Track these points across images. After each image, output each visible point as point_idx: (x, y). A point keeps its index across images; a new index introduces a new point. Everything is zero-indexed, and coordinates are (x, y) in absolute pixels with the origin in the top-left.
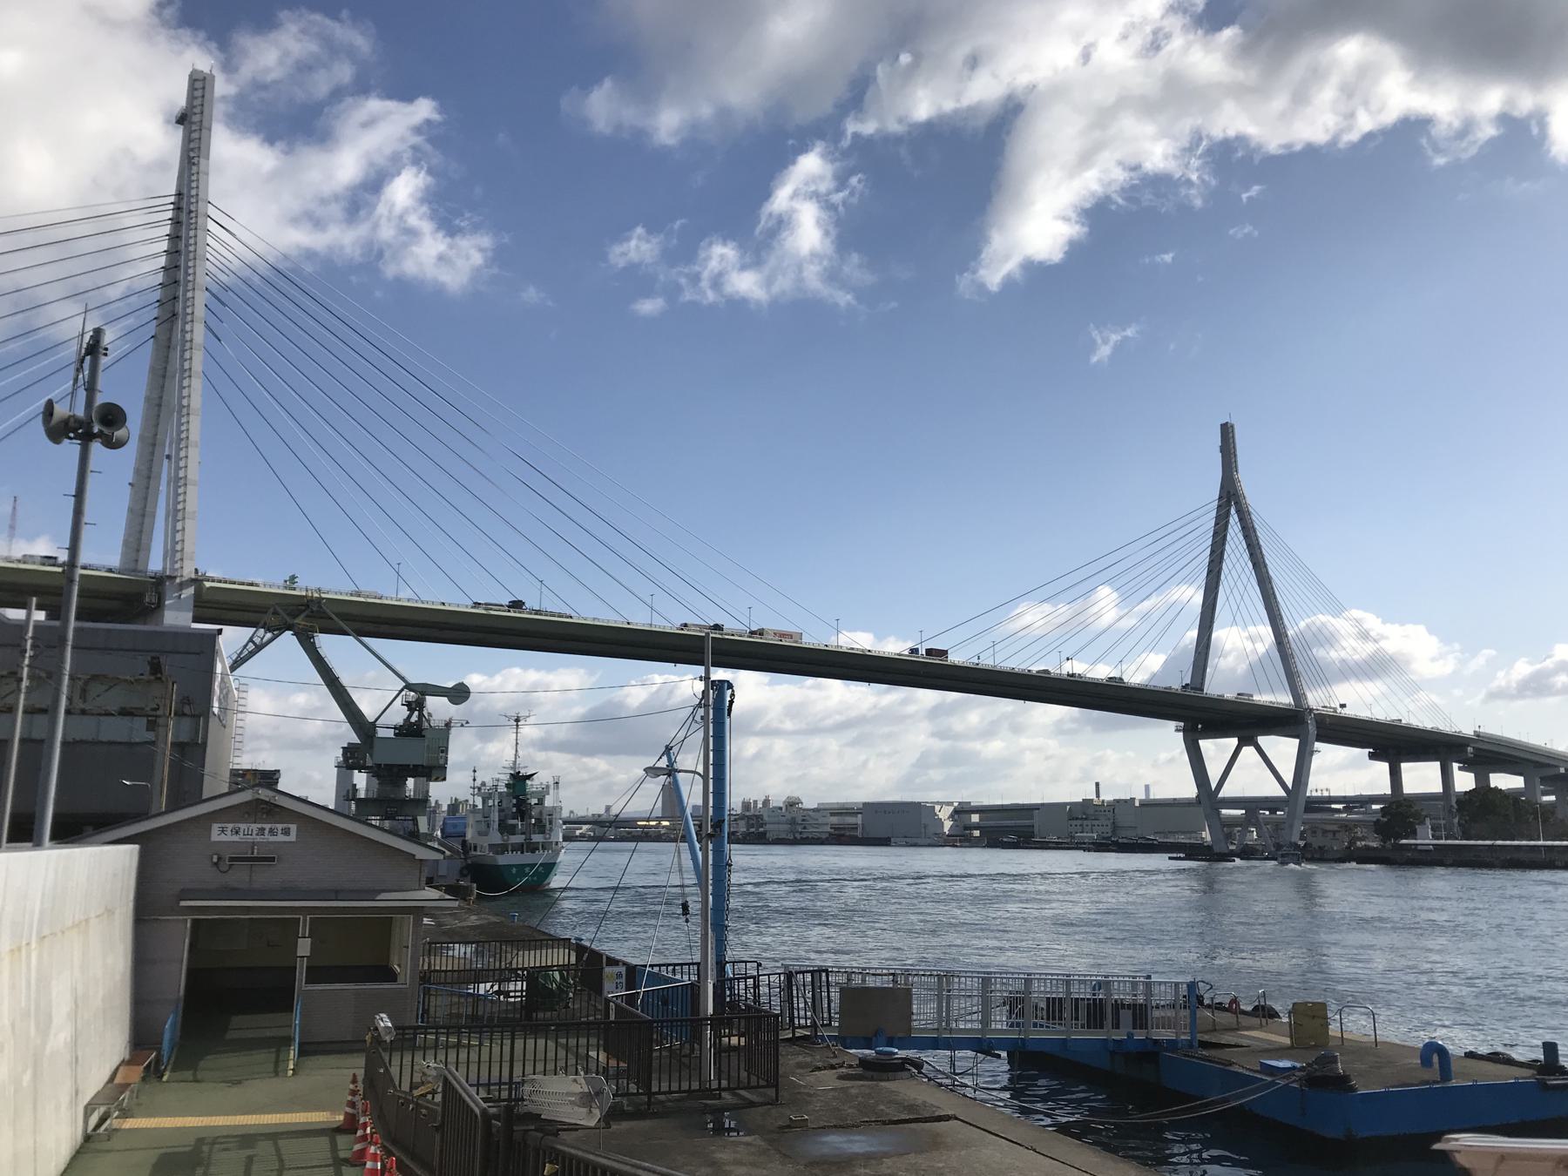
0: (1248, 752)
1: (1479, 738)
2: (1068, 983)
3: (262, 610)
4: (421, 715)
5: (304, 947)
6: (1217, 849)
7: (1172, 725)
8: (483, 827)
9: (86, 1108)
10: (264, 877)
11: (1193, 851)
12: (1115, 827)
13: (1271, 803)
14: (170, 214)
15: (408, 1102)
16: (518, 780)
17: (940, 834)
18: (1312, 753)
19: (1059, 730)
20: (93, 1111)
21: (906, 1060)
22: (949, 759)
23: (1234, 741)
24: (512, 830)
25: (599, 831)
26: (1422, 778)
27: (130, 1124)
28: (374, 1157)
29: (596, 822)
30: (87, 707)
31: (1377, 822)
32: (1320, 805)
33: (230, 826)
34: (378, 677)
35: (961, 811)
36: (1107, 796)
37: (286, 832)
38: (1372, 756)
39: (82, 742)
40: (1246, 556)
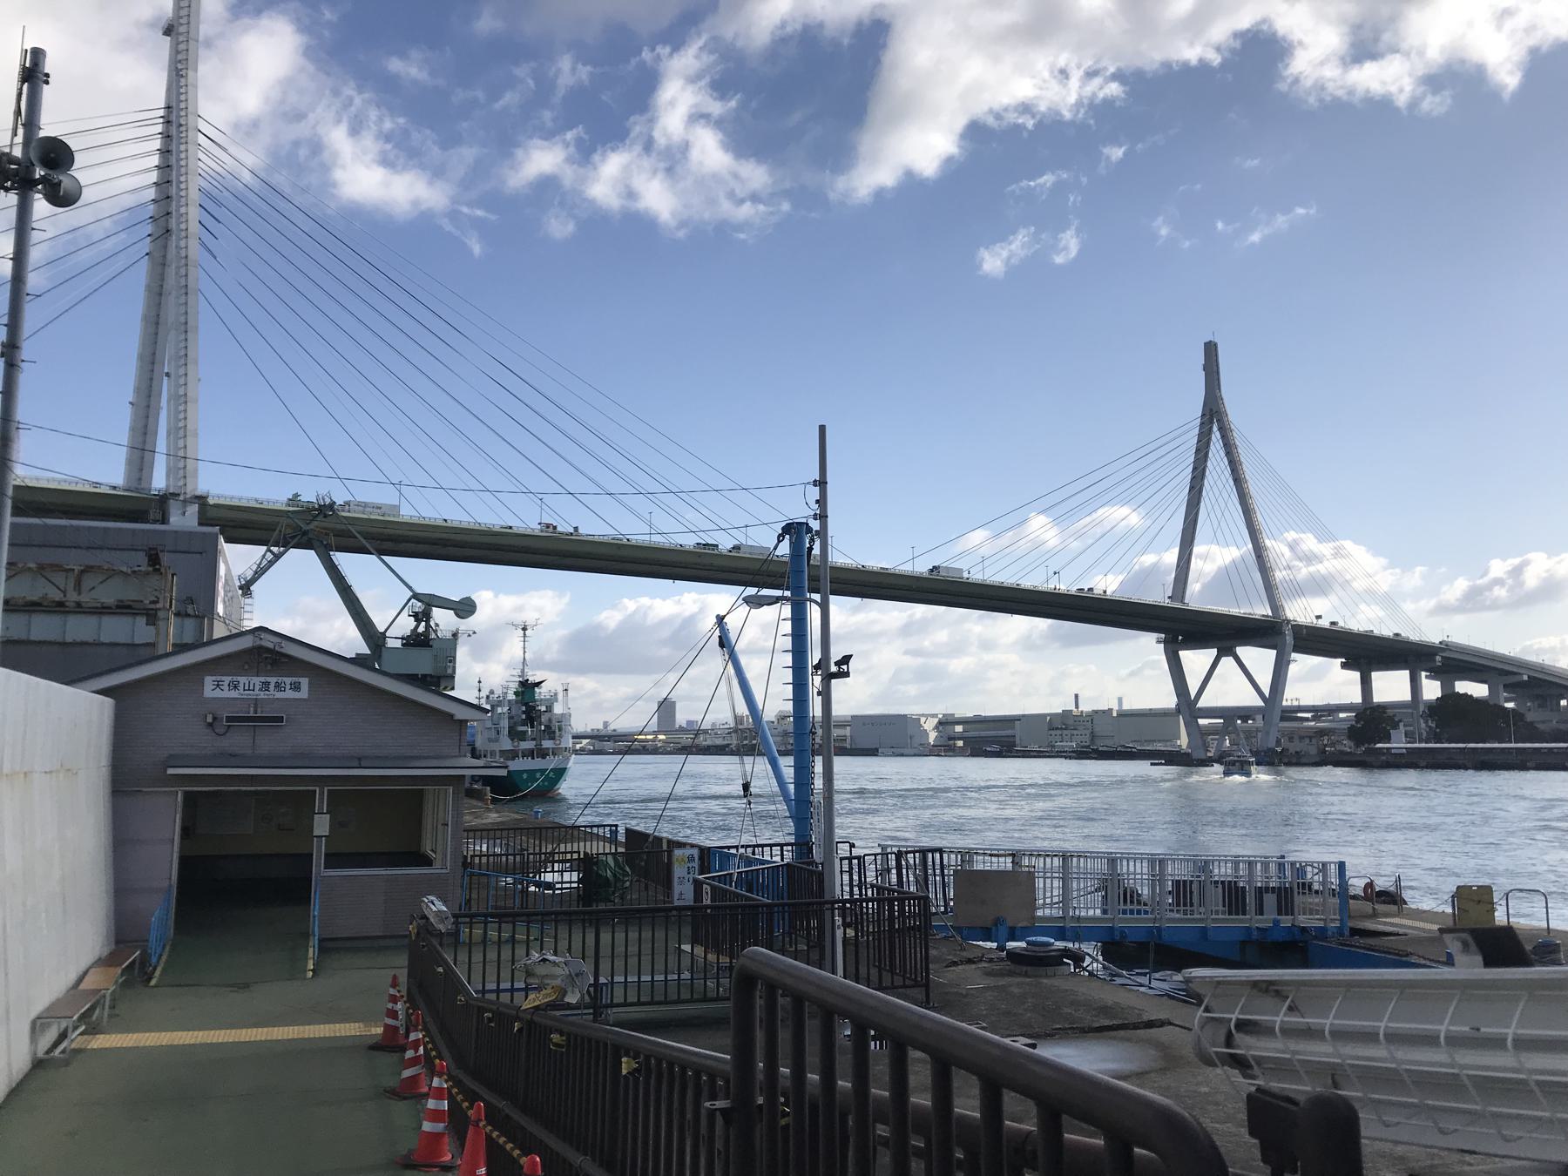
0: (1227, 662)
1: (1445, 647)
2: (1236, 864)
3: (270, 528)
4: (428, 626)
5: (322, 825)
6: (1196, 755)
7: (1155, 635)
8: (493, 734)
9: (34, 1023)
10: (268, 742)
11: (1173, 758)
12: (1093, 736)
13: (1245, 713)
14: (159, 128)
15: (481, 1010)
16: (527, 688)
17: (924, 745)
18: (1289, 663)
19: (1027, 645)
20: (45, 1027)
21: (1066, 953)
22: (922, 675)
23: (1214, 651)
24: (522, 736)
25: (599, 745)
26: (1392, 686)
27: (100, 1042)
28: (439, 1094)
29: (596, 737)
30: (85, 598)
31: (1351, 729)
32: (1290, 714)
33: (227, 679)
34: (387, 589)
35: (945, 723)
36: (1085, 707)
37: (296, 687)
38: (1344, 666)
39: (86, 643)
40: (1227, 472)
